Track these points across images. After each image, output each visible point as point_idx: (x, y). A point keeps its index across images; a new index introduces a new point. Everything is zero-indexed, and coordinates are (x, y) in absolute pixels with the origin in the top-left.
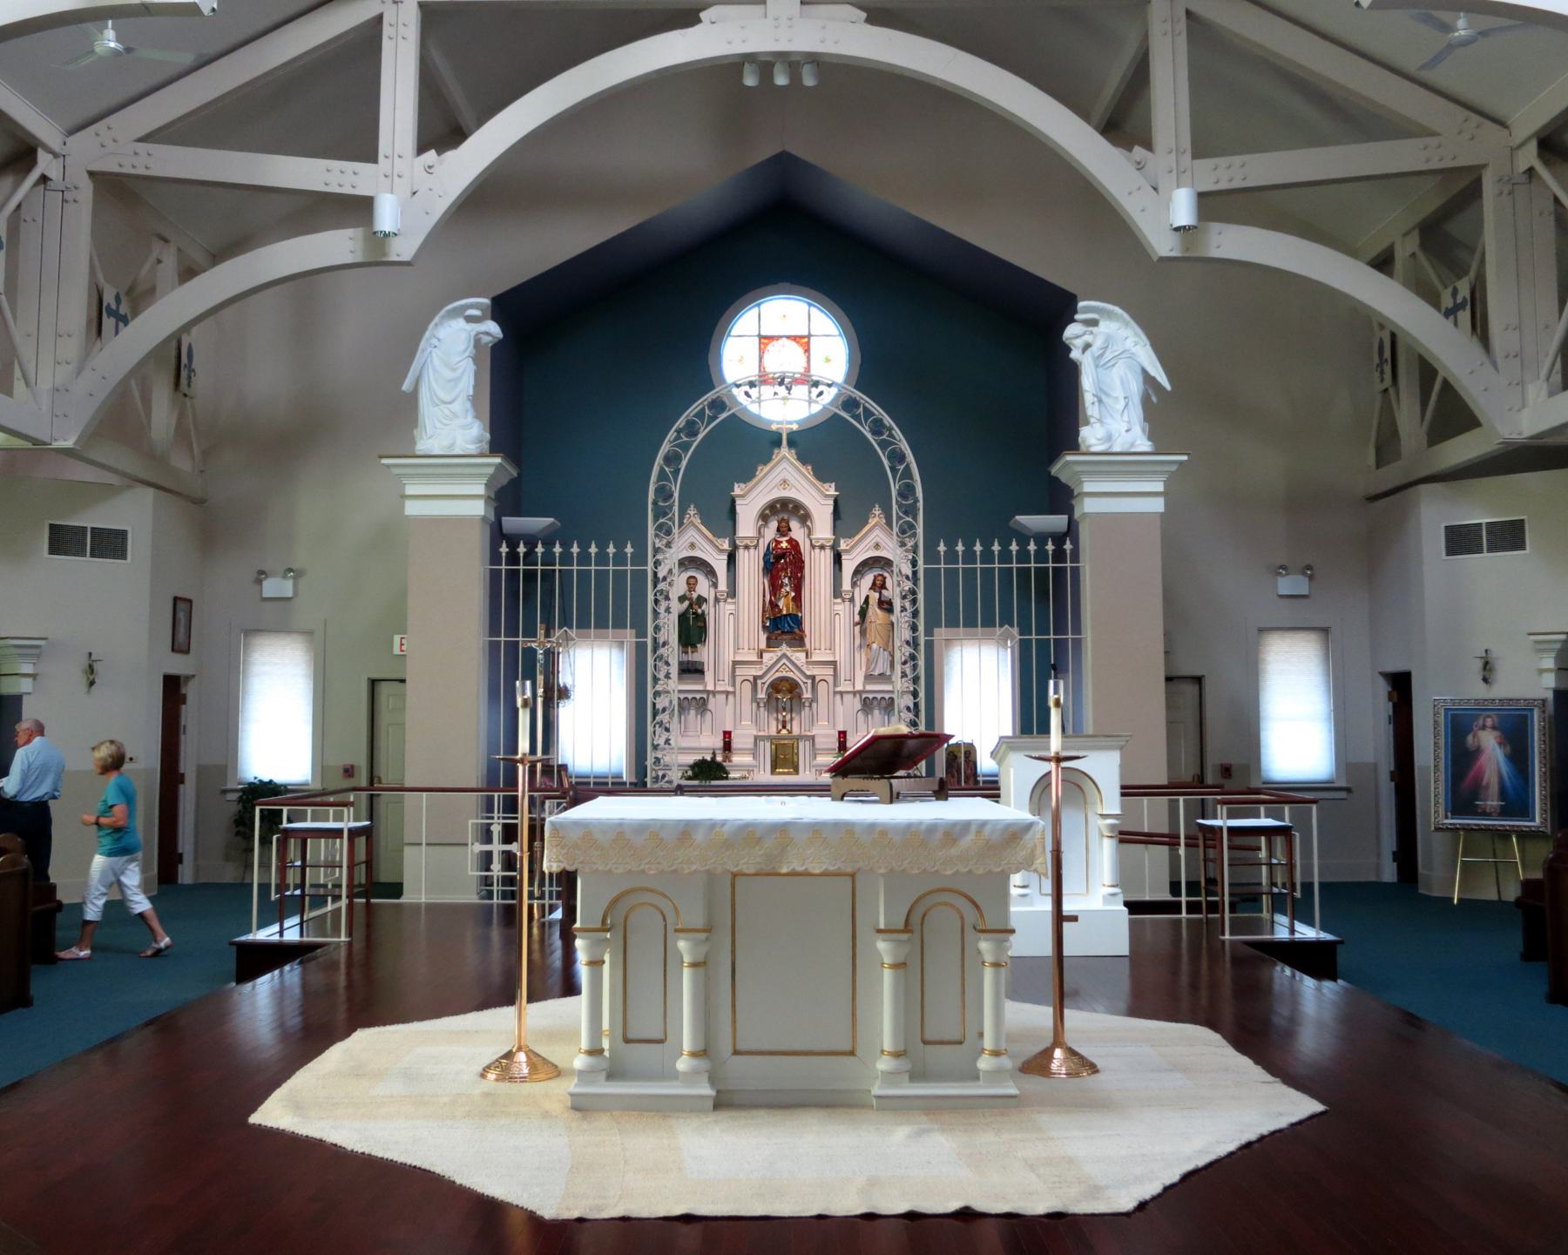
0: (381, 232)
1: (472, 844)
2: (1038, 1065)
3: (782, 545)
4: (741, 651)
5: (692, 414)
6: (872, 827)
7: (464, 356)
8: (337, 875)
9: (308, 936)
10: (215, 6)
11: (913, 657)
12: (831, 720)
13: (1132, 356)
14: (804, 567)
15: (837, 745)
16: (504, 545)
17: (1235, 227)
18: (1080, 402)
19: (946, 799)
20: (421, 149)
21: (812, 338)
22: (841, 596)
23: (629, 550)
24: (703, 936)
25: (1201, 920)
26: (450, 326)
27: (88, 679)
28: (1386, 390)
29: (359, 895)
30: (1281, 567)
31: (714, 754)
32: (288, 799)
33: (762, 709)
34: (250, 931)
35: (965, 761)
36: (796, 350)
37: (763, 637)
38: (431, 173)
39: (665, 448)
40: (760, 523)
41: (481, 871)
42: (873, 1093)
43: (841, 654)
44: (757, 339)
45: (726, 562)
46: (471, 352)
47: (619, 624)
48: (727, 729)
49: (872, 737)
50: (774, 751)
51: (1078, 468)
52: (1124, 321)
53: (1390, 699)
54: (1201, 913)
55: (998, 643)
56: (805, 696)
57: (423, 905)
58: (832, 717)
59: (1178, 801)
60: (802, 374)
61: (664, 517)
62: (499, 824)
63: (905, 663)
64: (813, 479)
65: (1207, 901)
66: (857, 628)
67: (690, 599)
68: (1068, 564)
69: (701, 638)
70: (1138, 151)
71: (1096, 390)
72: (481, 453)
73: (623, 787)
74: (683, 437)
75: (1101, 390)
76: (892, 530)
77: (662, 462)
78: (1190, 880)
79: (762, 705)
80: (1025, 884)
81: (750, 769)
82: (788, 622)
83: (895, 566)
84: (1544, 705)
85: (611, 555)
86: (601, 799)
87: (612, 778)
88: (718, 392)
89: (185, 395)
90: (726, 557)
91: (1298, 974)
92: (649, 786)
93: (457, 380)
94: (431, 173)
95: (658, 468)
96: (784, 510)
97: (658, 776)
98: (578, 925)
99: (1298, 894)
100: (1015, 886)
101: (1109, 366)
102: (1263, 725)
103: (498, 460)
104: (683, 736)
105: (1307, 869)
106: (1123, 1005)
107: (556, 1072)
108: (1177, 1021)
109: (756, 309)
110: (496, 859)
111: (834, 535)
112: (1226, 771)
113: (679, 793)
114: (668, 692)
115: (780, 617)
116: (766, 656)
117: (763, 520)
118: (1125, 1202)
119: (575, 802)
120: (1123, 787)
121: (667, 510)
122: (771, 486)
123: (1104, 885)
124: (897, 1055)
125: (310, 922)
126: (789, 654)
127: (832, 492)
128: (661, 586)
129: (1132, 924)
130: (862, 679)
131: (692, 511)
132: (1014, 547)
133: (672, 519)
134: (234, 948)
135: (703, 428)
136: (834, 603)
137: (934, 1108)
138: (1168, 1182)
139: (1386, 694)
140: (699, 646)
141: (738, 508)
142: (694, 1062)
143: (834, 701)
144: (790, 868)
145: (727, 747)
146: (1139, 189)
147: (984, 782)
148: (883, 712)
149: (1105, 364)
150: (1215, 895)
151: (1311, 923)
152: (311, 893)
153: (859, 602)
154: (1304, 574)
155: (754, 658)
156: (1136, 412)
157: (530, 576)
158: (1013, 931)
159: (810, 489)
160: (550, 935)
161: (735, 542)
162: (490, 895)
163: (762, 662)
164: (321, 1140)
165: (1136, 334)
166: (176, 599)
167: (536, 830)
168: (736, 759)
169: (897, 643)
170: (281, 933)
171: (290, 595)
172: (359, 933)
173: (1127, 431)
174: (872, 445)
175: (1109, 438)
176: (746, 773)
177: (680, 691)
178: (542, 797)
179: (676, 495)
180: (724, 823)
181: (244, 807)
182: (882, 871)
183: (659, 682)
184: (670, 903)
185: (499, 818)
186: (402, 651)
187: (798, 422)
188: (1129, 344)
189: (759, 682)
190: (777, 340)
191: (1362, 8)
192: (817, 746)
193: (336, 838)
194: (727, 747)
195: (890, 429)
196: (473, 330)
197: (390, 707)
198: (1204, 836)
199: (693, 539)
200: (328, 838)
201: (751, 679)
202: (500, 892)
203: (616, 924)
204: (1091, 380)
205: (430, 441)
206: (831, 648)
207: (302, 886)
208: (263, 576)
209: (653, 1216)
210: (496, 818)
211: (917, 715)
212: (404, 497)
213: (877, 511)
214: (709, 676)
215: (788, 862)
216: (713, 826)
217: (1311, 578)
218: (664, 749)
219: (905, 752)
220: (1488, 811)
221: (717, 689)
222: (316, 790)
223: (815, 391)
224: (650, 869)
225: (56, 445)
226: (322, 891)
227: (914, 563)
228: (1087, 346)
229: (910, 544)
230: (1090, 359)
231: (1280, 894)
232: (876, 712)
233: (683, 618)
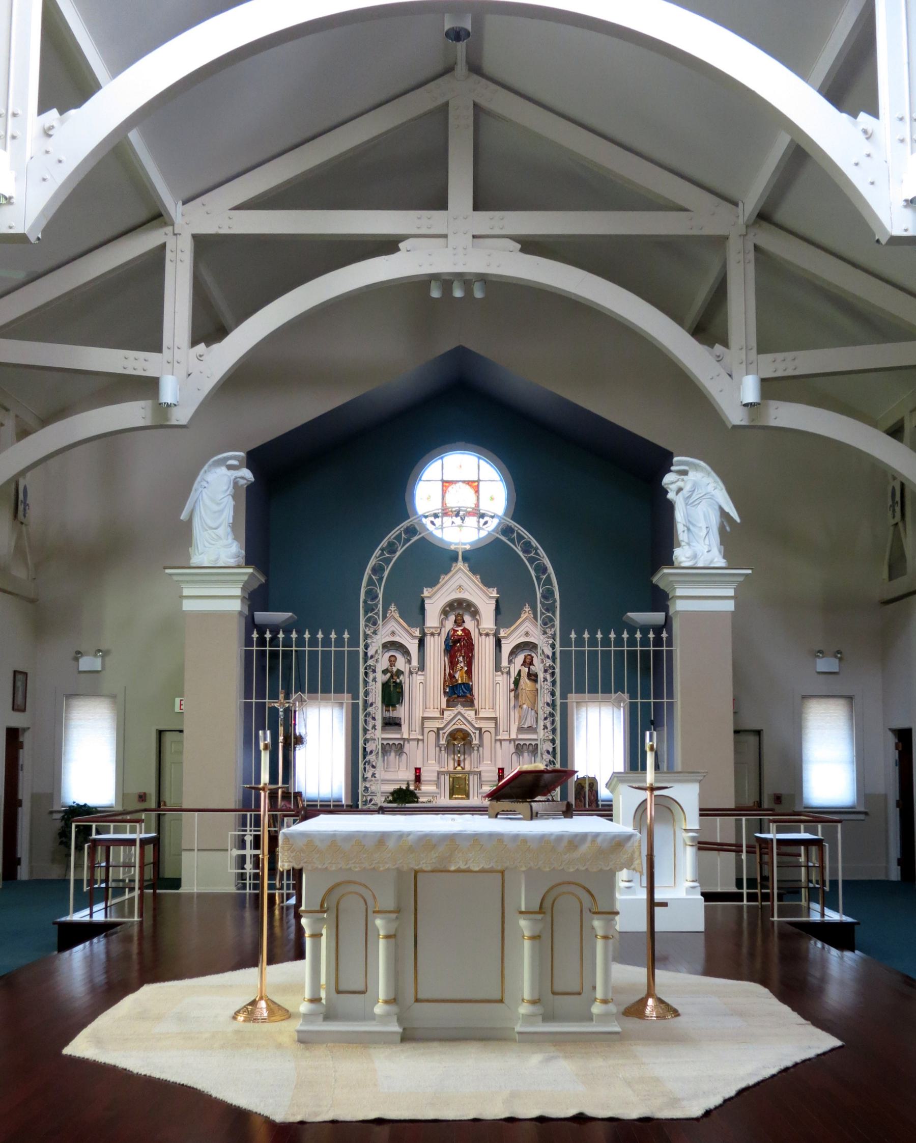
0: (165, 403)
1: (231, 850)
2: (636, 1010)
3: (458, 633)
4: (428, 710)
5: (392, 538)
6: (516, 837)
7: (226, 495)
8: (132, 873)
9: (111, 917)
10: (40, 236)
11: (552, 715)
12: (493, 759)
13: (712, 498)
15: (497, 778)
16: (255, 632)
17: (788, 404)
18: (675, 528)
19: (572, 817)
20: (194, 343)
21: (481, 483)
22: (501, 670)
23: (346, 636)
24: (394, 916)
25: (757, 906)
26: (216, 473)
28: (897, 524)
29: (148, 887)
30: (820, 652)
31: (408, 785)
32: (98, 817)
33: (443, 752)
34: (67, 914)
35: (589, 790)
36: (469, 491)
37: (444, 700)
38: (202, 360)
39: (372, 562)
40: (443, 617)
41: (238, 869)
42: (516, 1030)
43: (501, 712)
44: (440, 483)
45: (417, 645)
46: (230, 492)
47: (339, 690)
48: (418, 766)
49: (518, 772)
50: (451, 784)
51: (671, 578)
53: (897, 748)
54: (757, 901)
55: (613, 704)
57: (195, 894)
58: (493, 759)
59: (741, 820)
60: (473, 509)
61: (371, 612)
62: (251, 835)
63: (546, 719)
64: (480, 585)
65: (762, 893)
66: (512, 694)
67: (391, 672)
68: (665, 648)
70: (718, 348)
71: (686, 523)
72: (238, 565)
73: (328, 808)
75: (689, 521)
76: (537, 622)
77: (370, 572)
78: (748, 877)
79: (443, 749)
80: (630, 879)
81: (434, 795)
83: (539, 648)
85: (294, 639)
86: (322, 816)
87: (333, 801)
88: (411, 521)
89: (22, 523)
90: (417, 642)
91: (826, 946)
92: (360, 807)
93: (222, 511)
94: (202, 360)
95: (368, 576)
97: (366, 800)
98: (303, 908)
99: (827, 889)
100: (622, 881)
101: (695, 504)
102: (804, 766)
103: (250, 570)
104: (386, 771)
105: (834, 870)
106: (700, 965)
107: (288, 1015)
108: (738, 979)
109: (440, 461)
110: (248, 859)
111: (496, 626)
112: (778, 799)
113: (381, 812)
114: (375, 740)
115: (456, 685)
117: (444, 615)
118: (695, 1110)
119: (305, 818)
120: (701, 810)
121: (374, 607)
123: (687, 880)
124: (533, 1002)
125: (112, 907)
126: (463, 712)
127: (495, 594)
128: (370, 662)
129: (707, 908)
131: (393, 608)
132: (625, 635)
133: (377, 614)
134: (56, 926)
135: (400, 548)
136: (496, 676)
137: (560, 1041)
138: (727, 1096)
139: (894, 745)
140: (397, 706)
142: (387, 1008)
144: (457, 867)
145: (418, 779)
147: (602, 805)
148: (530, 754)
150: (768, 888)
151: (836, 909)
152: (113, 886)
153: (514, 674)
154: (836, 657)
156: (715, 538)
157: (274, 655)
158: (617, 913)
160: (287, 915)
162: (244, 888)
163: (443, 717)
164: (115, 1066)
166: (15, 673)
167: (274, 840)
168: (424, 788)
169: (540, 704)
170: (91, 915)
171: (99, 669)
172: (148, 915)
173: (708, 551)
174: (523, 560)
175: (695, 556)
176: (431, 798)
177: (383, 739)
178: (282, 815)
179: (380, 596)
180: (409, 834)
181: (66, 824)
182: (524, 869)
183: (368, 732)
184: (370, 892)
185: (251, 831)
186: (181, 709)
187: (470, 544)
188: (710, 488)
189: (441, 732)
190: (455, 483)
191: (882, 244)
192: (483, 779)
193: (133, 846)
194: (418, 779)
195: (536, 549)
196: (232, 476)
197: (173, 751)
198: (760, 845)
200: (126, 846)
201: (435, 730)
202: (252, 884)
204: (682, 515)
205: (201, 556)
206: (494, 708)
207: (106, 880)
208: (80, 655)
209: (354, 1119)
210: (248, 831)
211: (554, 757)
212: (182, 597)
213: (527, 608)
214: (405, 727)
215: (455, 863)
216: (401, 836)
217: (840, 659)
218: (372, 781)
219: (542, 783)
221: (411, 737)
222: (118, 811)
223: (482, 521)
224: (355, 867)
226: (121, 884)
227: (553, 646)
228: (680, 490)
229: (550, 632)
231: (815, 888)
232: (526, 754)
233: (385, 686)
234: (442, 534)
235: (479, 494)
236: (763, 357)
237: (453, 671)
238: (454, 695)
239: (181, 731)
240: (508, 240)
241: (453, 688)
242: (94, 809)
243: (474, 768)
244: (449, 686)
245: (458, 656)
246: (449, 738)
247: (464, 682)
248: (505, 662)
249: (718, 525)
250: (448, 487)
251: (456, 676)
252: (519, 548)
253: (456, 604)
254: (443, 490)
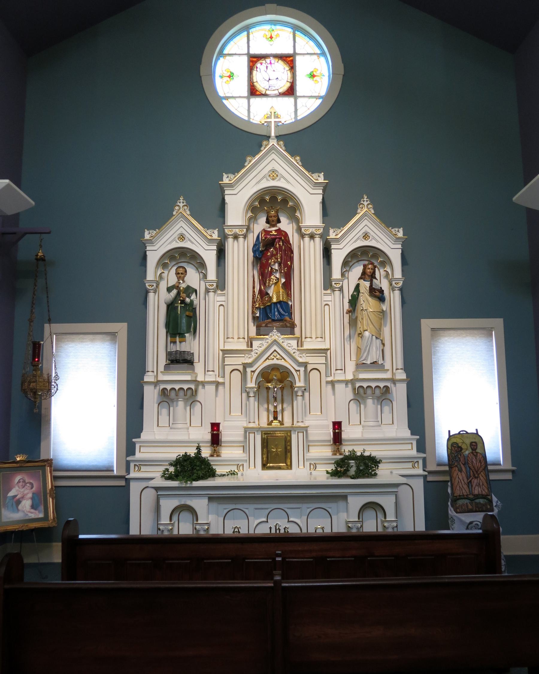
31: (198, 448)
33: (252, 399)
40: (250, 214)
56: (298, 384)
66: (347, 317)
79: (252, 394)
116: (256, 344)
117: (252, 212)
126: (280, 341)
127: (321, 180)
148: (376, 401)
155: (244, 347)
168: (226, 452)
176: (234, 468)
189: (249, 370)
192: (311, 438)
201: (241, 368)
221: (206, 380)
232: (370, 402)
233: (171, 306)
248: (336, 273)
250: (256, 62)
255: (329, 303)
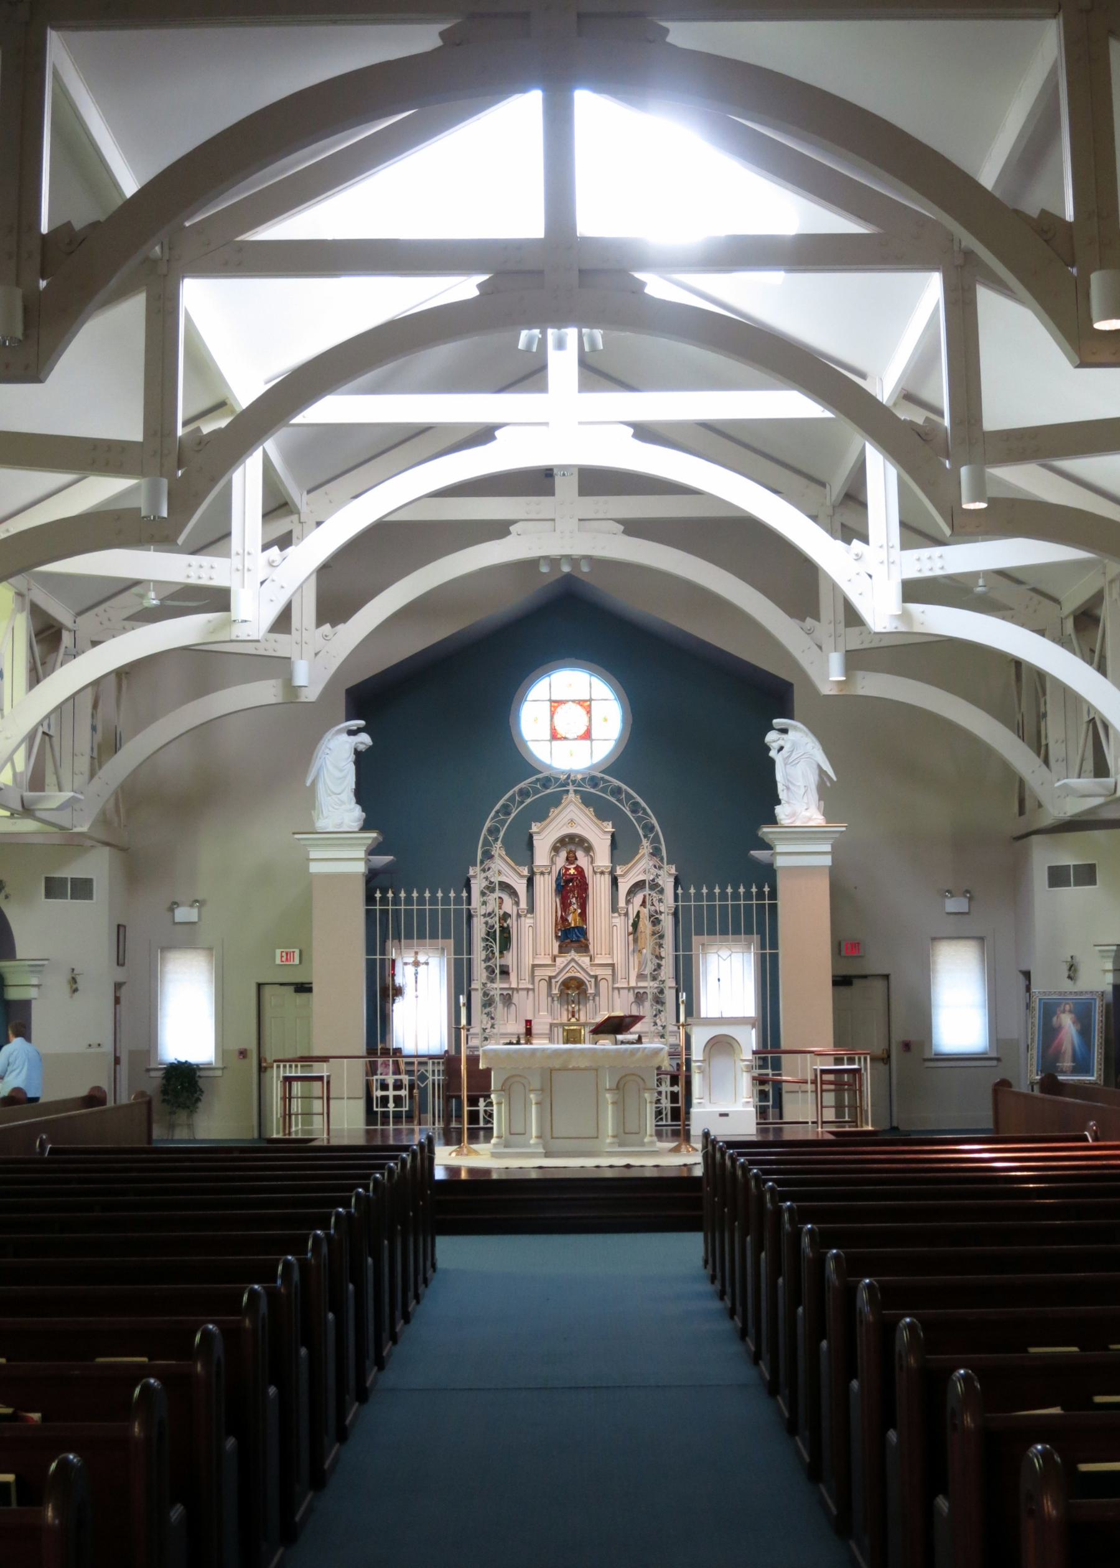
3: (570, 871)
14: (588, 888)
21: (593, 702)
24: (541, 1092)
27: (71, 987)
30: (948, 891)
33: (556, 1002)
37: (556, 944)
40: (553, 854)
43: (618, 958)
44: (548, 703)
45: (526, 885)
48: (529, 1018)
52: (805, 732)
66: (631, 937)
69: (507, 947)
70: (809, 622)
74: (500, 815)
75: (788, 780)
79: (555, 999)
80: (702, 1097)
82: (576, 933)
84: (1103, 995)
90: (526, 882)
93: (345, 777)
96: (571, 843)
101: (794, 764)
111: (612, 863)
112: (907, 1046)
115: (569, 929)
122: (560, 826)
124: (614, 1137)
126: (576, 958)
127: (610, 829)
130: (635, 978)
136: (612, 917)
140: (505, 952)
141: (535, 842)
143: (613, 994)
146: (809, 648)
149: (791, 762)
154: (966, 897)
155: (550, 962)
156: (813, 795)
159: (592, 827)
161: (532, 869)
163: (555, 965)
165: (813, 742)
166: (119, 926)
175: (794, 814)
182: (607, 1067)
186: (282, 961)
189: (553, 981)
199: (503, 869)
201: (547, 978)
203: (505, 1089)
204: (781, 774)
206: (611, 953)
208: (175, 906)
212: (309, 860)
217: (970, 899)
220: (1064, 1069)
221: (520, 987)
225: (76, 830)
228: (781, 748)
230: (781, 759)
234: (551, 760)
235: (591, 714)
236: (850, 630)
237: (565, 913)
238: (567, 939)
239: (303, 988)
240: (611, 521)
241: (566, 933)
242: (195, 1066)
243: (590, 1019)
244: (562, 931)
245: (571, 897)
246: (562, 987)
247: (578, 925)
248: (622, 903)
249: (817, 783)
250: (557, 707)
251: (568, 918)
252: (627, 808)
253: (567, 840)
254: (551, 711)
255: (617, 924)
